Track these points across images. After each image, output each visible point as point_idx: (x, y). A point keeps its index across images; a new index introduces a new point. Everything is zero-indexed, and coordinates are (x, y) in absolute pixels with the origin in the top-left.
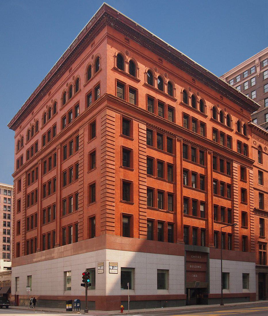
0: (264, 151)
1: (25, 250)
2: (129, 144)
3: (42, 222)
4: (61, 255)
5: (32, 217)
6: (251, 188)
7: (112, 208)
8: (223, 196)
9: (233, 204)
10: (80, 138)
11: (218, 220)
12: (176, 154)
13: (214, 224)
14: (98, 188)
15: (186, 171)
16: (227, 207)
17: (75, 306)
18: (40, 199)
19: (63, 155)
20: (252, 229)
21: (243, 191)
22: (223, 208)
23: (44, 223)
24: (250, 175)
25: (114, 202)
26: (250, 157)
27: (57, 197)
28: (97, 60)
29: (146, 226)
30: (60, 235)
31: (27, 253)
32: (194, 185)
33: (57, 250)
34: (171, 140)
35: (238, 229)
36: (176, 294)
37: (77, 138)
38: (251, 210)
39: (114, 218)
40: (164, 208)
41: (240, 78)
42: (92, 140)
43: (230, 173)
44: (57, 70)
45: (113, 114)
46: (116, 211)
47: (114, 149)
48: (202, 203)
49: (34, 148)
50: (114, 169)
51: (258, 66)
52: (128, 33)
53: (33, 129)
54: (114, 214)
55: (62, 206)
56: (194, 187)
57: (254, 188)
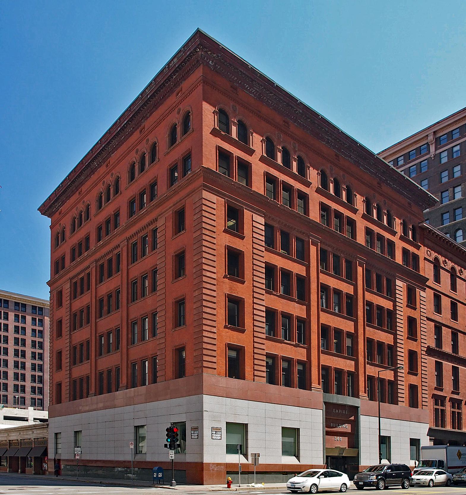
0: (442, 265)
1: (70, 393)
2: (237, 244)
3: (98, 353)
4: (130, 402)
5: (82, 345)
6: (422, 317)
7: (211, 335)
8: (380, 327)
9: (395, 339)
10: (158, 231)
11: (373, 360)
12: (309, 262)
13: (368, 366)
14: (189, 306)
15: (324, 288)
16: (386, 342)
17: (155, 476)
18: (94, 319)
19: (131, 256)
20: (423, 376)
21: (412, 322)
22: (380, 344)
23: (101, 354)
24: (421, 298)
25: (215, 327)
26: (421, 273)
27: (122, 317)
28: (186, 119)
29: (264, 363)
30: (127, 373)
31: (73, 397)
32: (337, 308)
33: (92, 400)
34: (302, 241)
35: (403, 375)
36: (311, 464)
37: (155, 231)
38: (423, 348)
39: (215, 351)
40: (291, 338)
41: (404, 159)
42: (179, 234)
43: (391, 294)
44: (119, 129)
45: (214, 198)
46: (218, 340)
47: (215, 250)
48: (349, 335)
49: (83, 244)
50: (215, 279)
51: (432, 144)
52: (236, 78)
53: (81, 216)
54: (215, 345)
55: (130, 331)
56: (337, 311)
57: (427, 317)
